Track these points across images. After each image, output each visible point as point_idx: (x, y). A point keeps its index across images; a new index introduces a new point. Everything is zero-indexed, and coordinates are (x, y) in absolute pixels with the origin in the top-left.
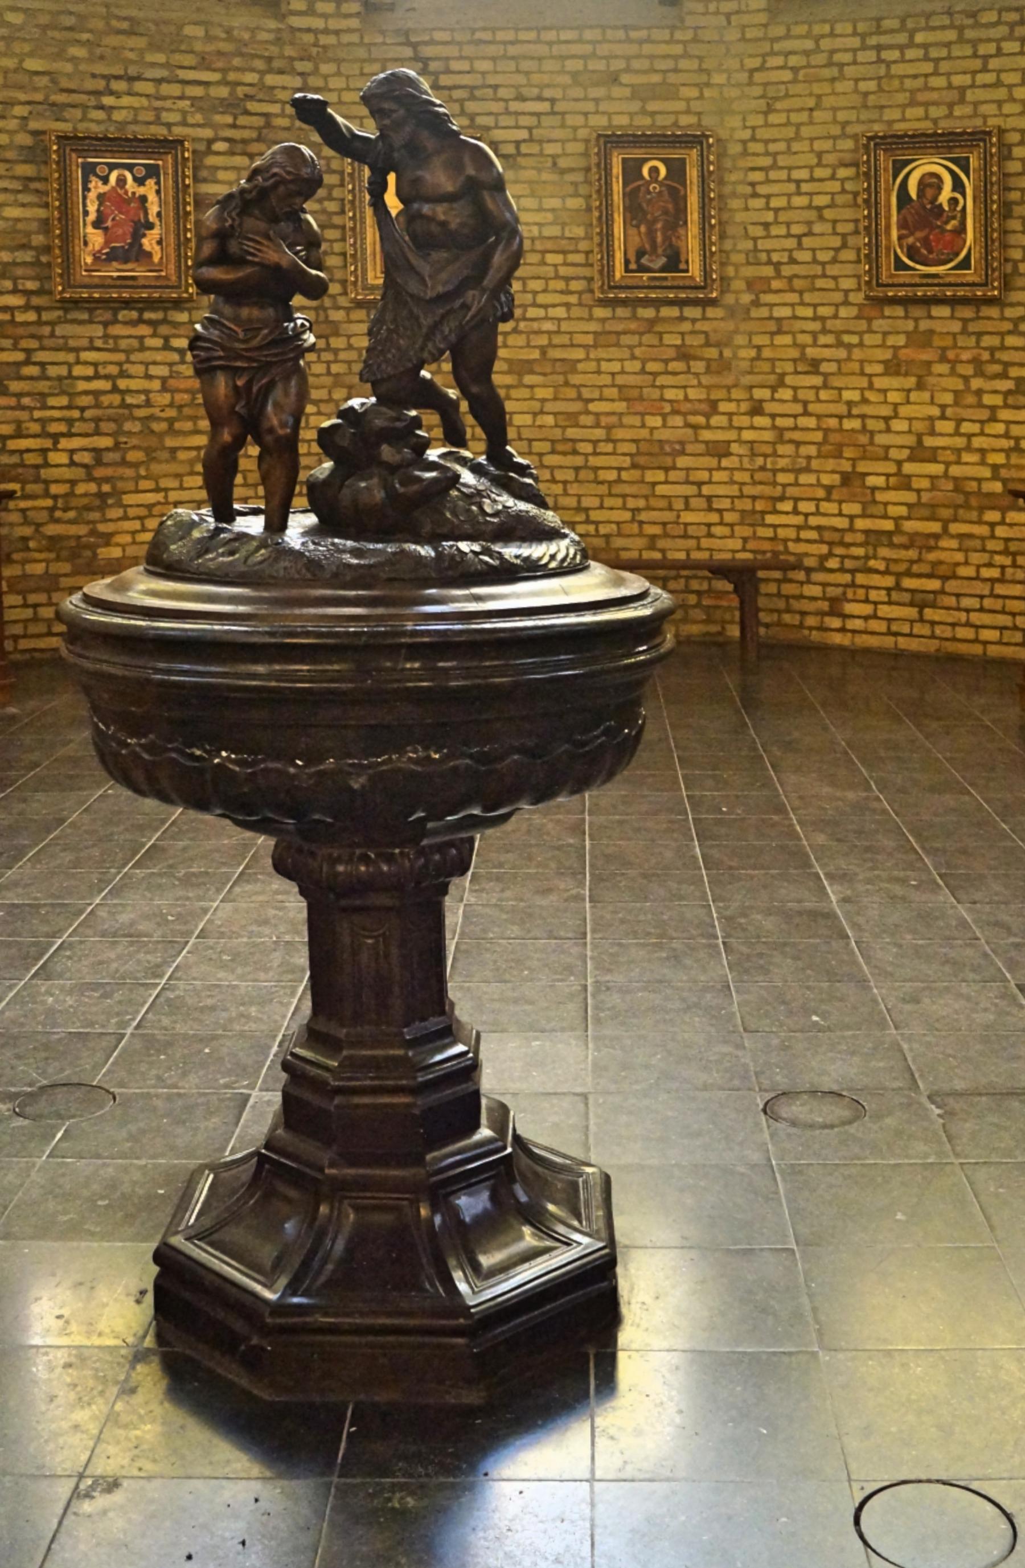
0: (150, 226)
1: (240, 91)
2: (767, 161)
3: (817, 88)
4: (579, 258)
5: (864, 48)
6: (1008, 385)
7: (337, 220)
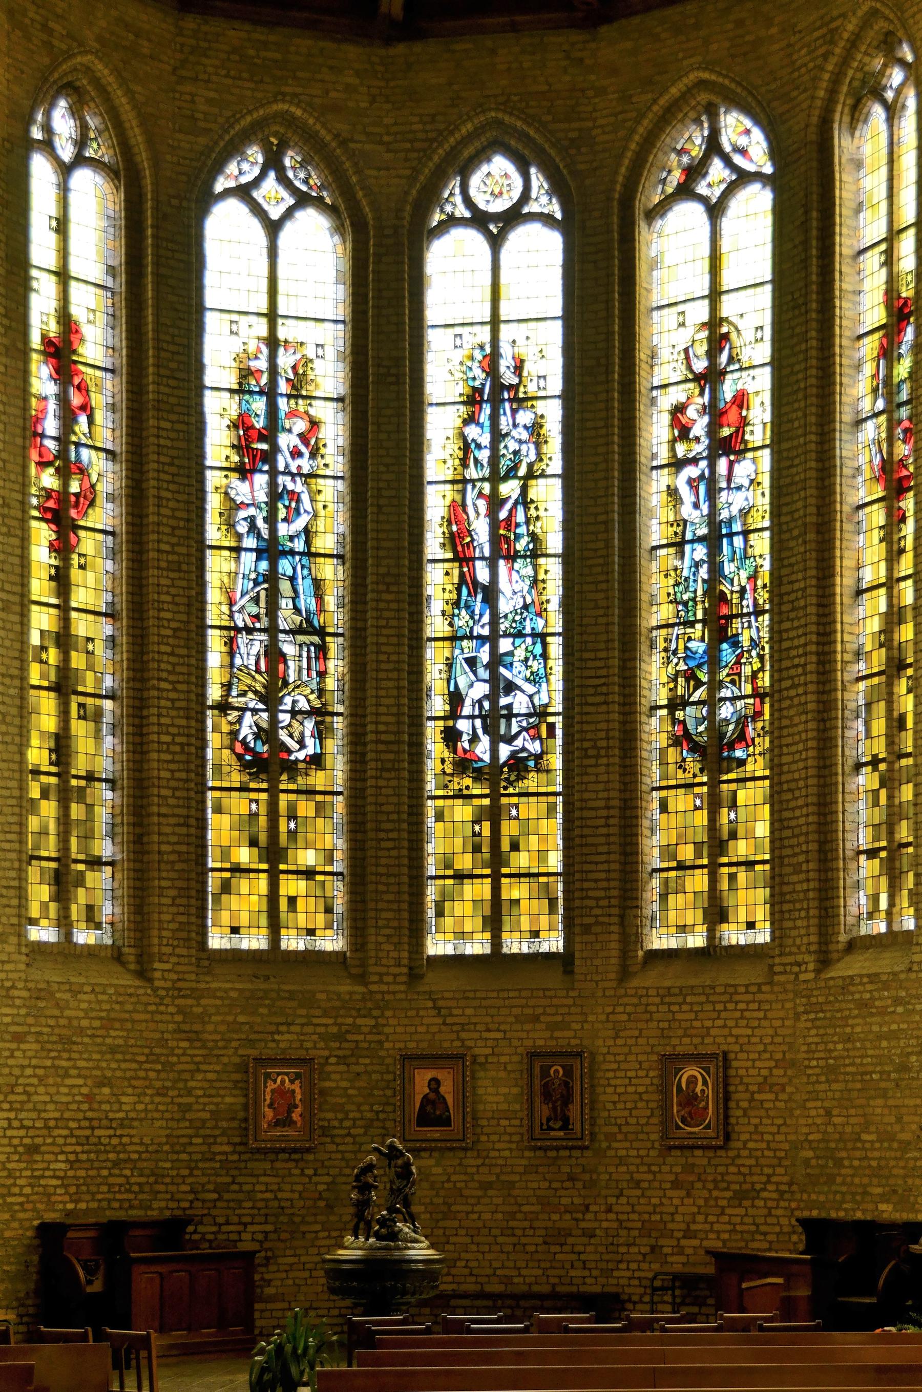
0: (296, 1107)
1: (344, 1028)
2: (615, 1066)
3: (640, 1026)
4: (517, 1122)
5: (663, 1003)
6: (730, 1194)
7: (392, 1100)
